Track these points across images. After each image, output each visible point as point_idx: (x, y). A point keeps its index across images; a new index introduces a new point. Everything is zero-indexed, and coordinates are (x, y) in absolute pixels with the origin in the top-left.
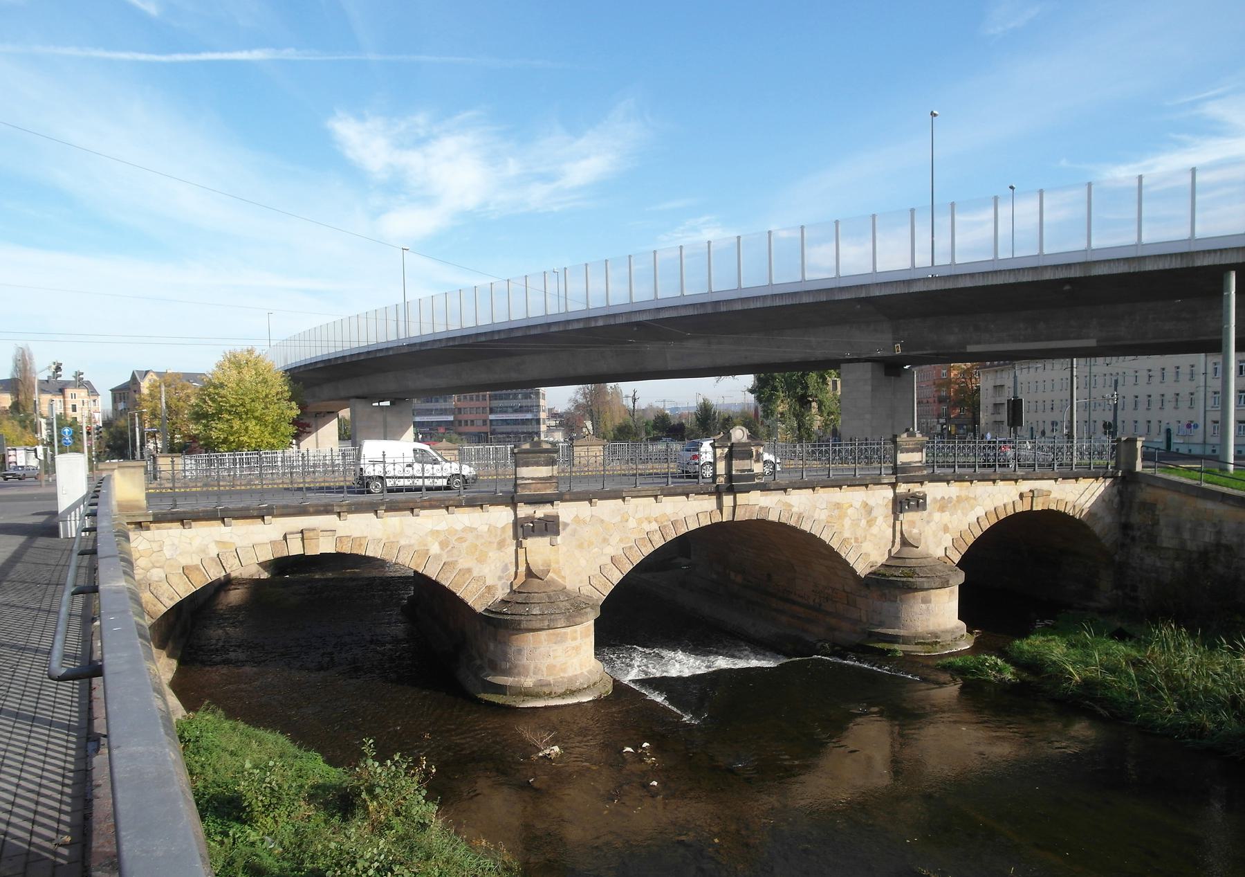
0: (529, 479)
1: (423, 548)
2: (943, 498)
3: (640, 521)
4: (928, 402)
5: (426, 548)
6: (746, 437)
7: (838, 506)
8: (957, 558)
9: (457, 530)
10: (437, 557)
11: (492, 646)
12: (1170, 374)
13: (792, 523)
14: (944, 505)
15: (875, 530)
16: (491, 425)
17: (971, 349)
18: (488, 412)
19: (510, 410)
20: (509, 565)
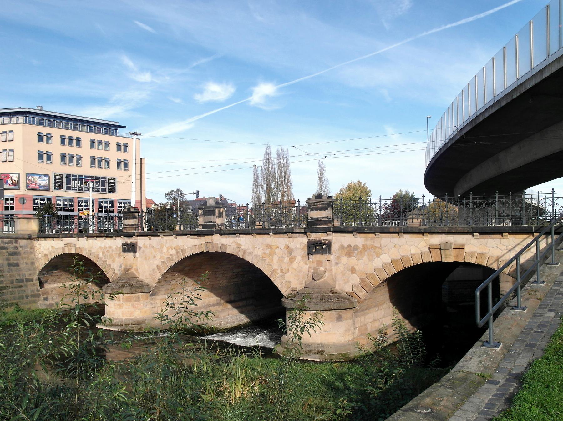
0: (126, 225)
2: (349, 246)
3: (168, 249)
7: (269, 247)
14: (350, 251)
15: (295, 265)
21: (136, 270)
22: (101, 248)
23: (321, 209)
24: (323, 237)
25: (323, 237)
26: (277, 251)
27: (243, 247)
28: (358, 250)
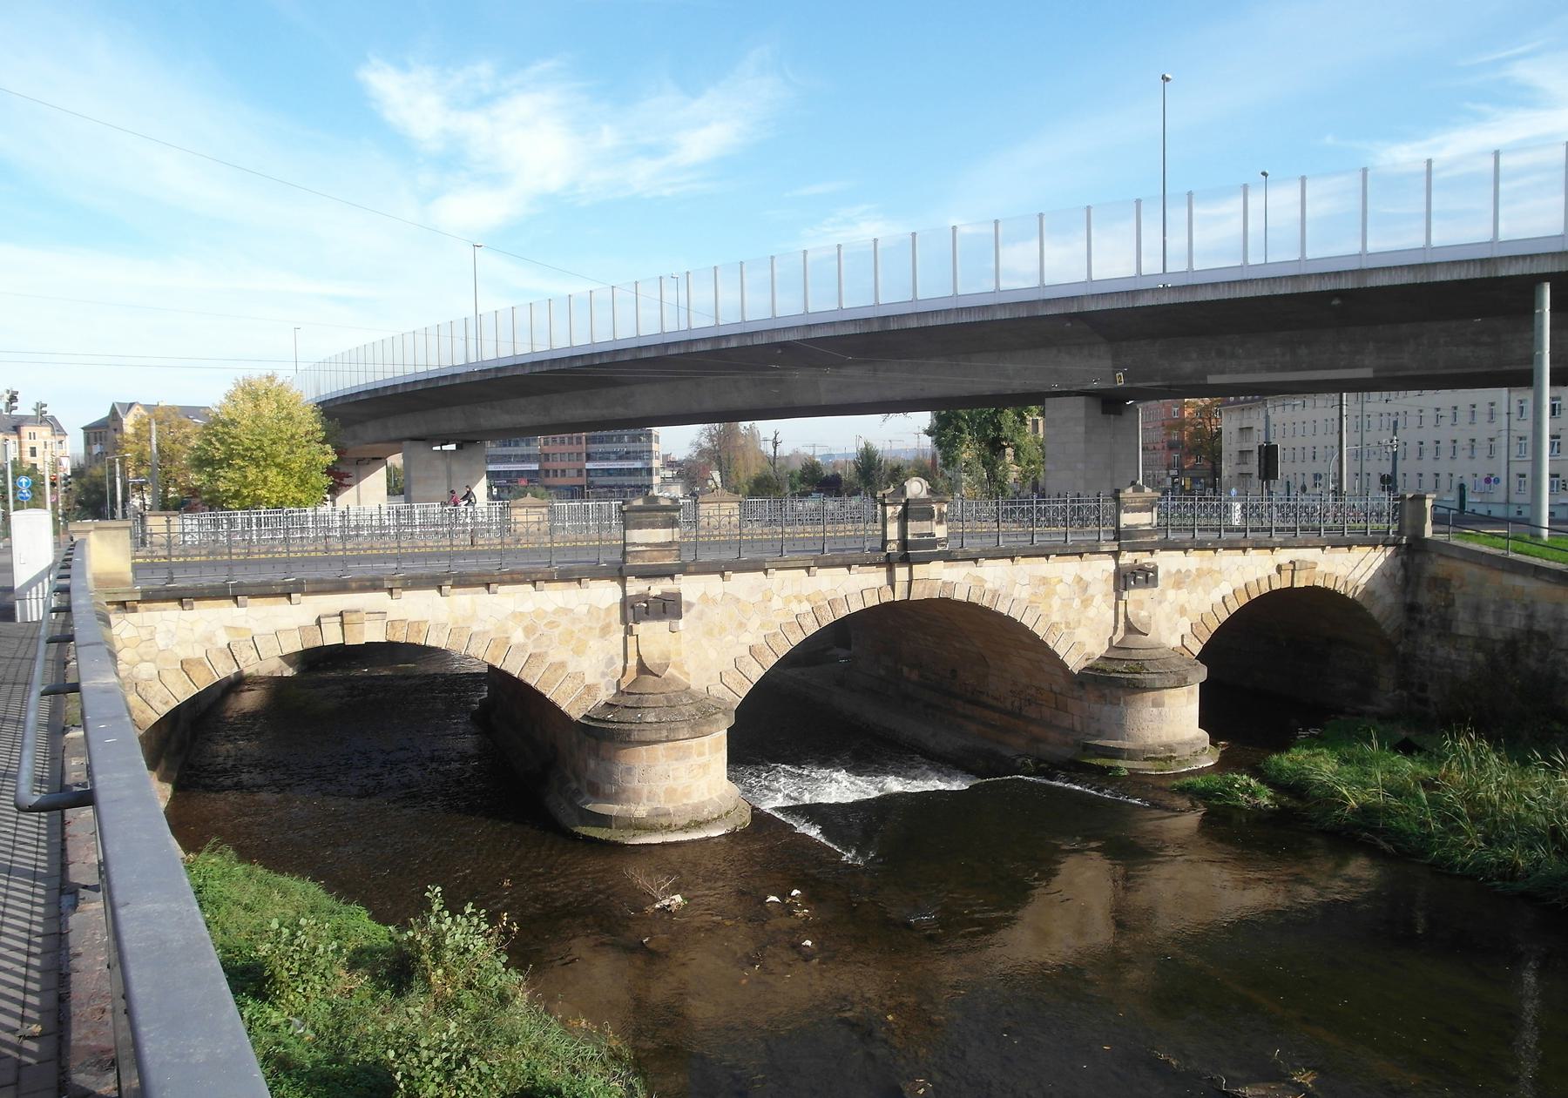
0: (641, 545)
1: (502, 635)
2: (1179, 571)
3: (787, 601)
4: (1154, 448)
5: (507, 636)
6: (925, 491)
7: (1044, 581)
8: (1197, 648)
9: (546, 613)
10: (521, 647)
11: (592, 764)
12: (1463, 416)
13: (985, 603)
14: (1180, 580)
15: (1092, 612)
16: (588, 475)
17: (1212, 379)
18: (585, 458)
19: (613, 456)
20: (616, 658)
21: (679, 667)
22: (516, 616)
23: (1140, 510)
24: (1144, 558)
25: (1144, 558)
26: (1059, 588)
27: (988, 586)
28: (1191, 578)
